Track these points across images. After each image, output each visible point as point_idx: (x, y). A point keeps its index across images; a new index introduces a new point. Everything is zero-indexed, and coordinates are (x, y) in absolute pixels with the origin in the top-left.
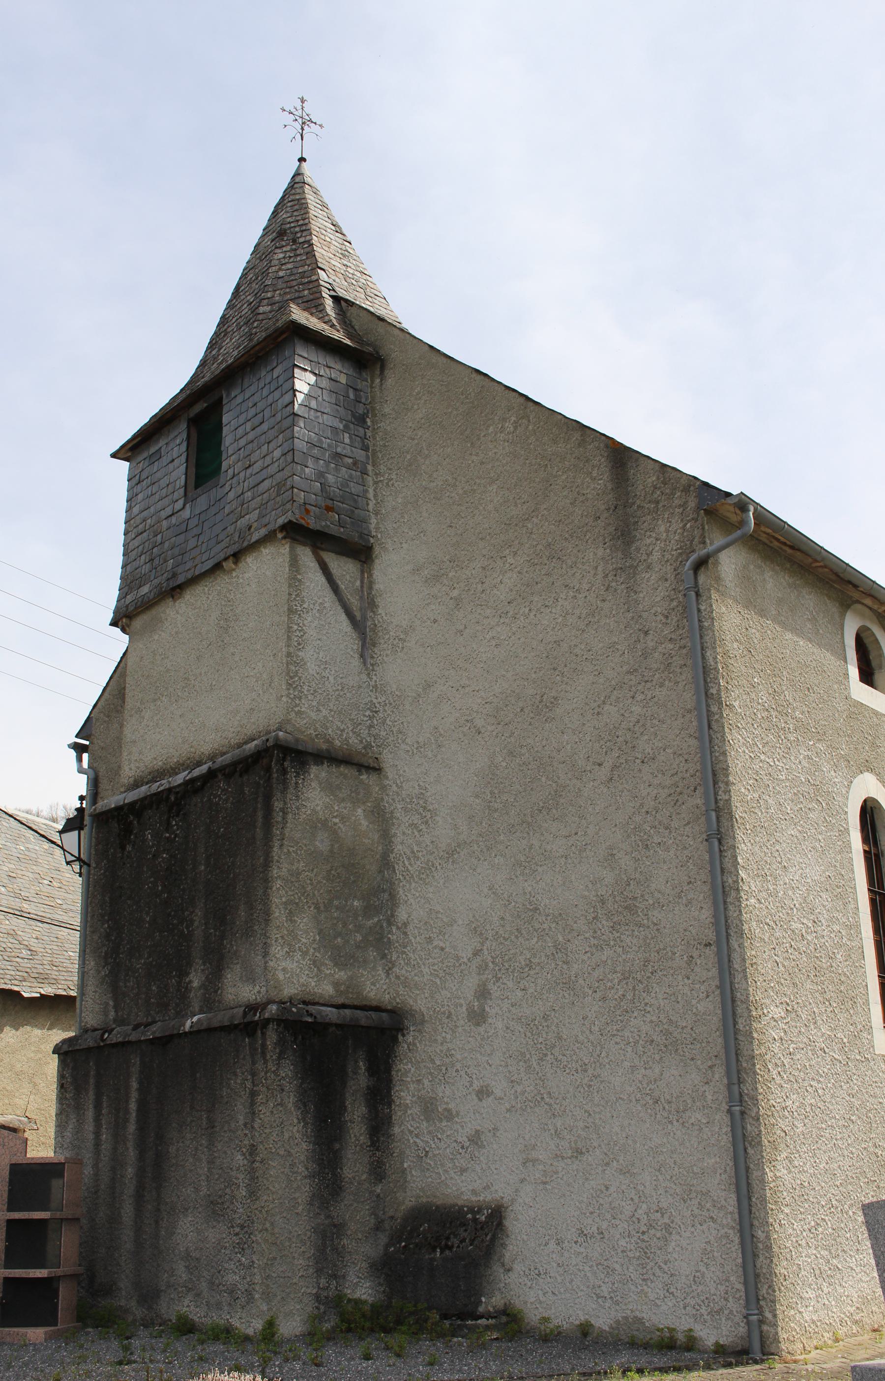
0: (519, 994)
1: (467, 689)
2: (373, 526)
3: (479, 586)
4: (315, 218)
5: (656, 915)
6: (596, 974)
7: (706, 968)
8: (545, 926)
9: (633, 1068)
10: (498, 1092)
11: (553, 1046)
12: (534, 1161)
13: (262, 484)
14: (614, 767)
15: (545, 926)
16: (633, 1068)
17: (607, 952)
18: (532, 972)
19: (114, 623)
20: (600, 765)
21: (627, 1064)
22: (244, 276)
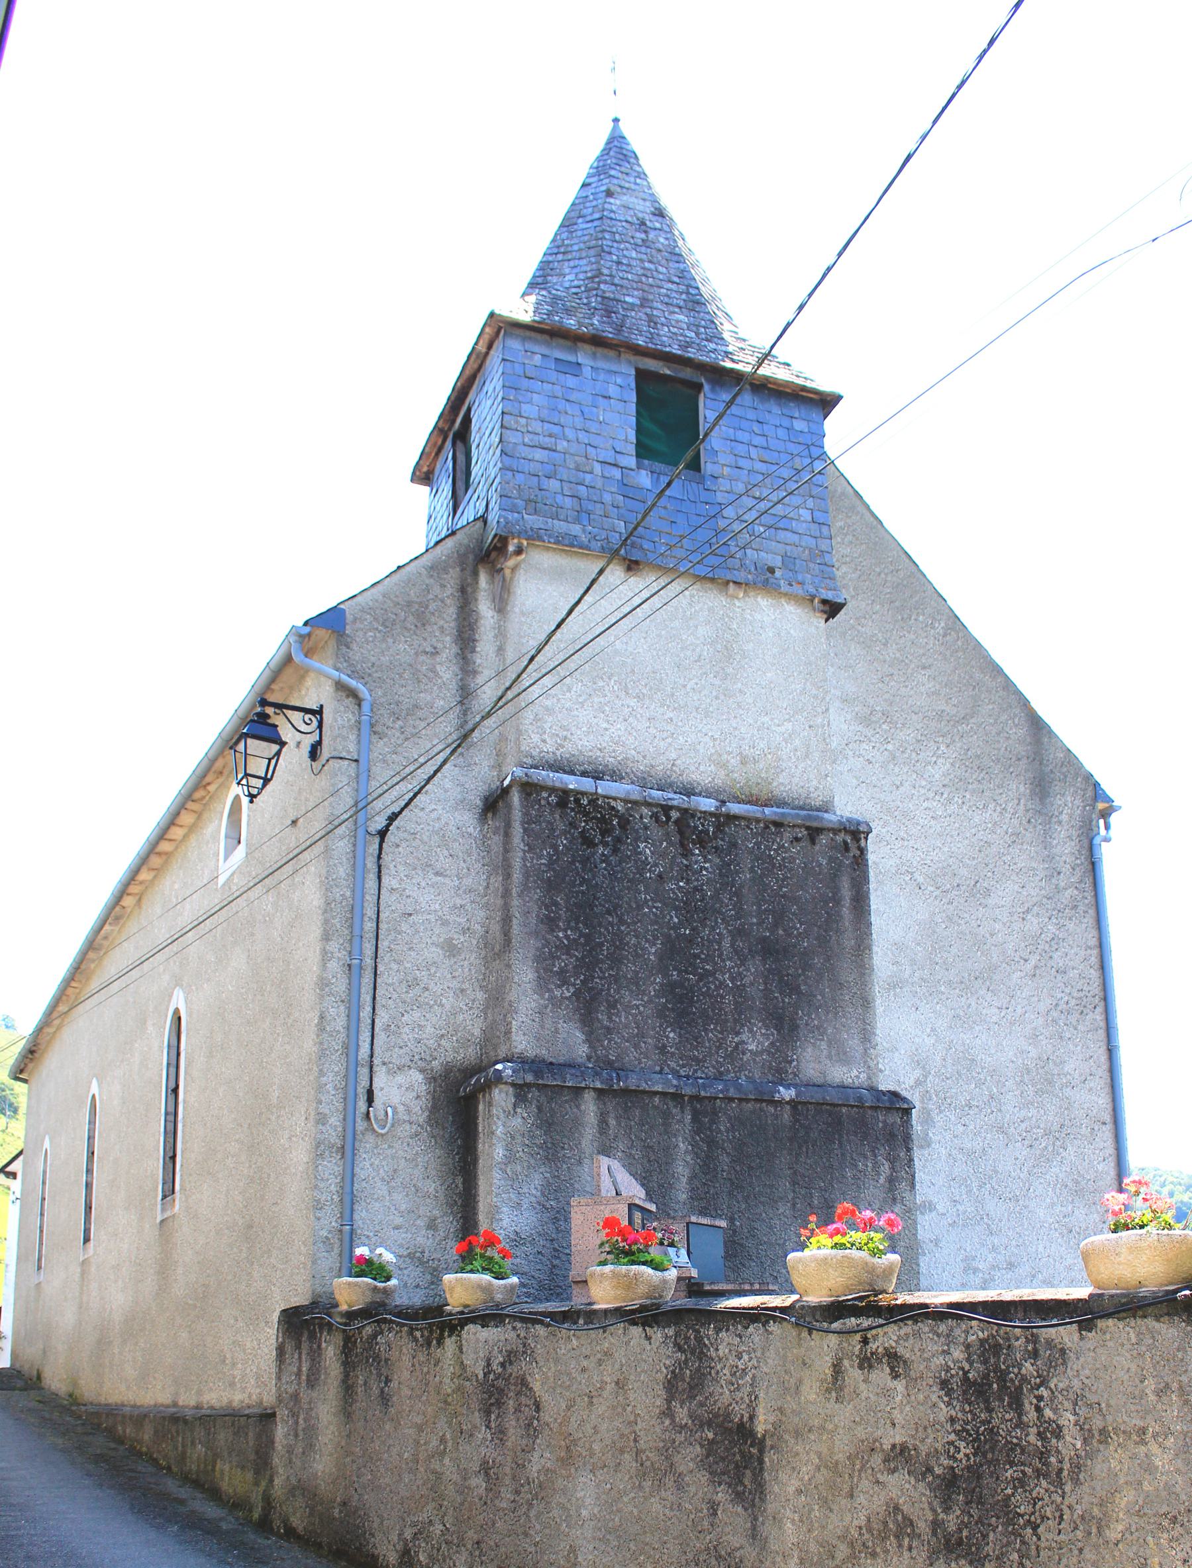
0: (961, 1128)
1: (906, 843)
2: (375, 1525)
3: (914, 755)
4: (205, 1198)
5: (1068, 1092)
6: (1023, 1126)
7: (1107, 1133)
8: (982, 1076)
9: (1053, 1205)
10: (940, 1208)
11: (991, 1178)
12: (976, 1270)
13: (368, 1040)
14: (1036, 967)
15: (982, 1076)
16: (1053, 1205)
17: (1033, 1112)
18: (971, 1112)
19: (492, 315)
20: (1026, 961)
21: (1048, 1200)
22: (568, 224)
